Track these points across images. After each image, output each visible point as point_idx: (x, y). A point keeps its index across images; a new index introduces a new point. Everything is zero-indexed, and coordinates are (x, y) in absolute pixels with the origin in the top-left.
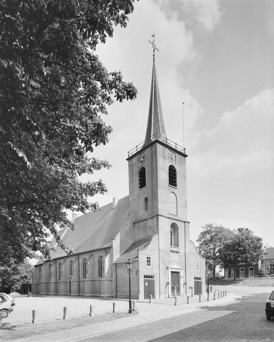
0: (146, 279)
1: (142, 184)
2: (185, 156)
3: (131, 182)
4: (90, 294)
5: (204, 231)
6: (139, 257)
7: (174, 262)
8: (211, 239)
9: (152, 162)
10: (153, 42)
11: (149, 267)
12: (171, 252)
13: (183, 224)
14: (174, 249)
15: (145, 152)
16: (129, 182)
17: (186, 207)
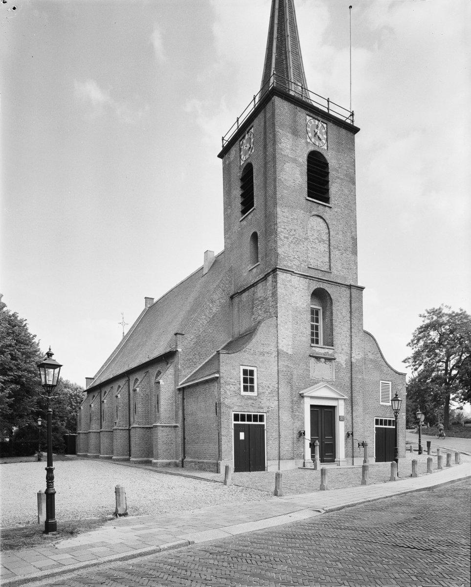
1: (247, 203)
2: (355, 130)
3: (228, 204)
4: (141, 457)
5: (425, 323)
7: (320, 384)
8: (440, 339)
9: (265, 147)
11: (249, 393)
12: (313, 359)
13: (346, 292)
14: (320, 351)
15: (252, 126)
16: (224, 205)
17: (355, 253)
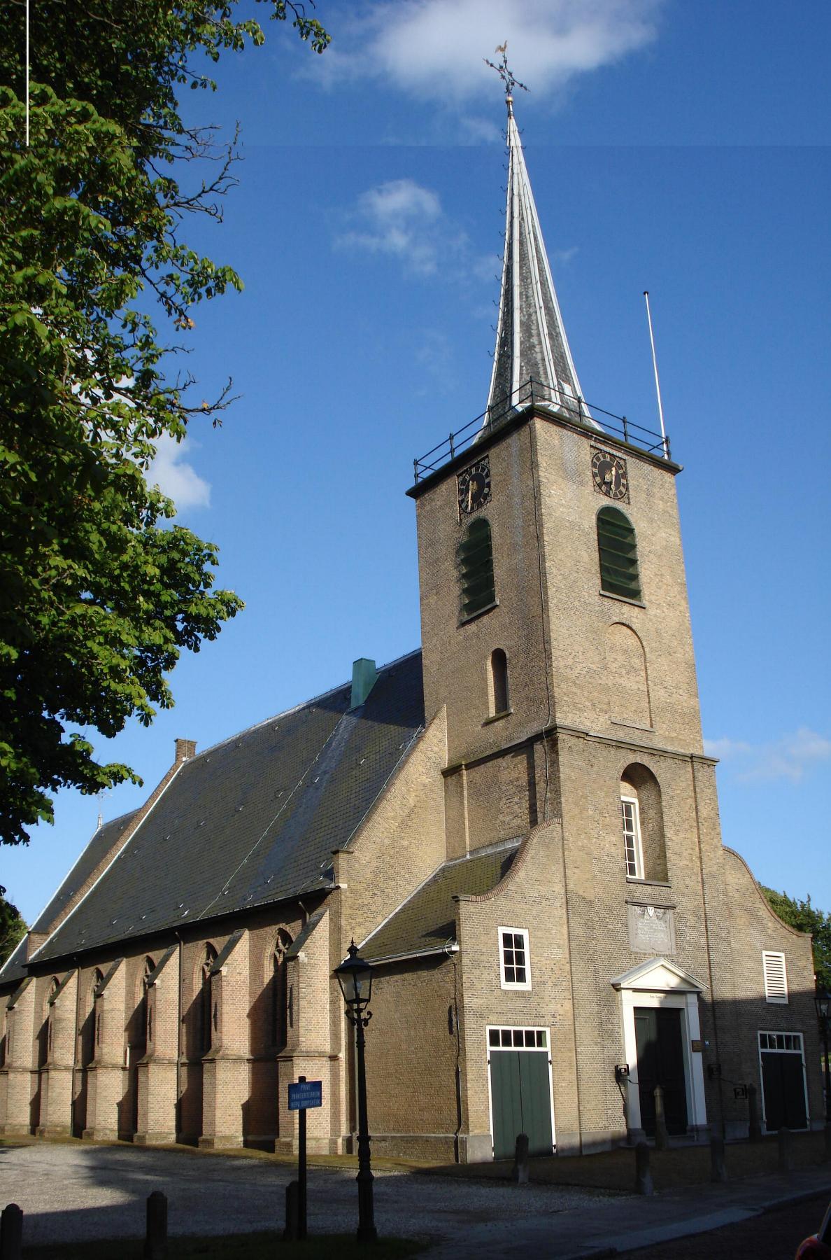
0: (501, 1048)
3: (429, 589)
6: (465, 929)
11: (516, 986)
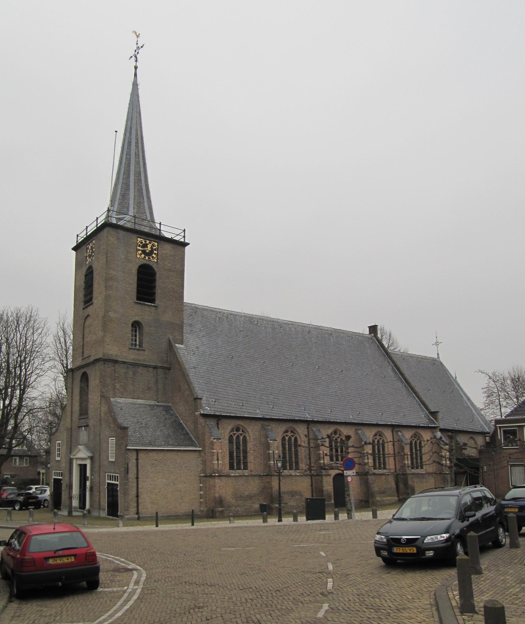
10: (140, 47)
